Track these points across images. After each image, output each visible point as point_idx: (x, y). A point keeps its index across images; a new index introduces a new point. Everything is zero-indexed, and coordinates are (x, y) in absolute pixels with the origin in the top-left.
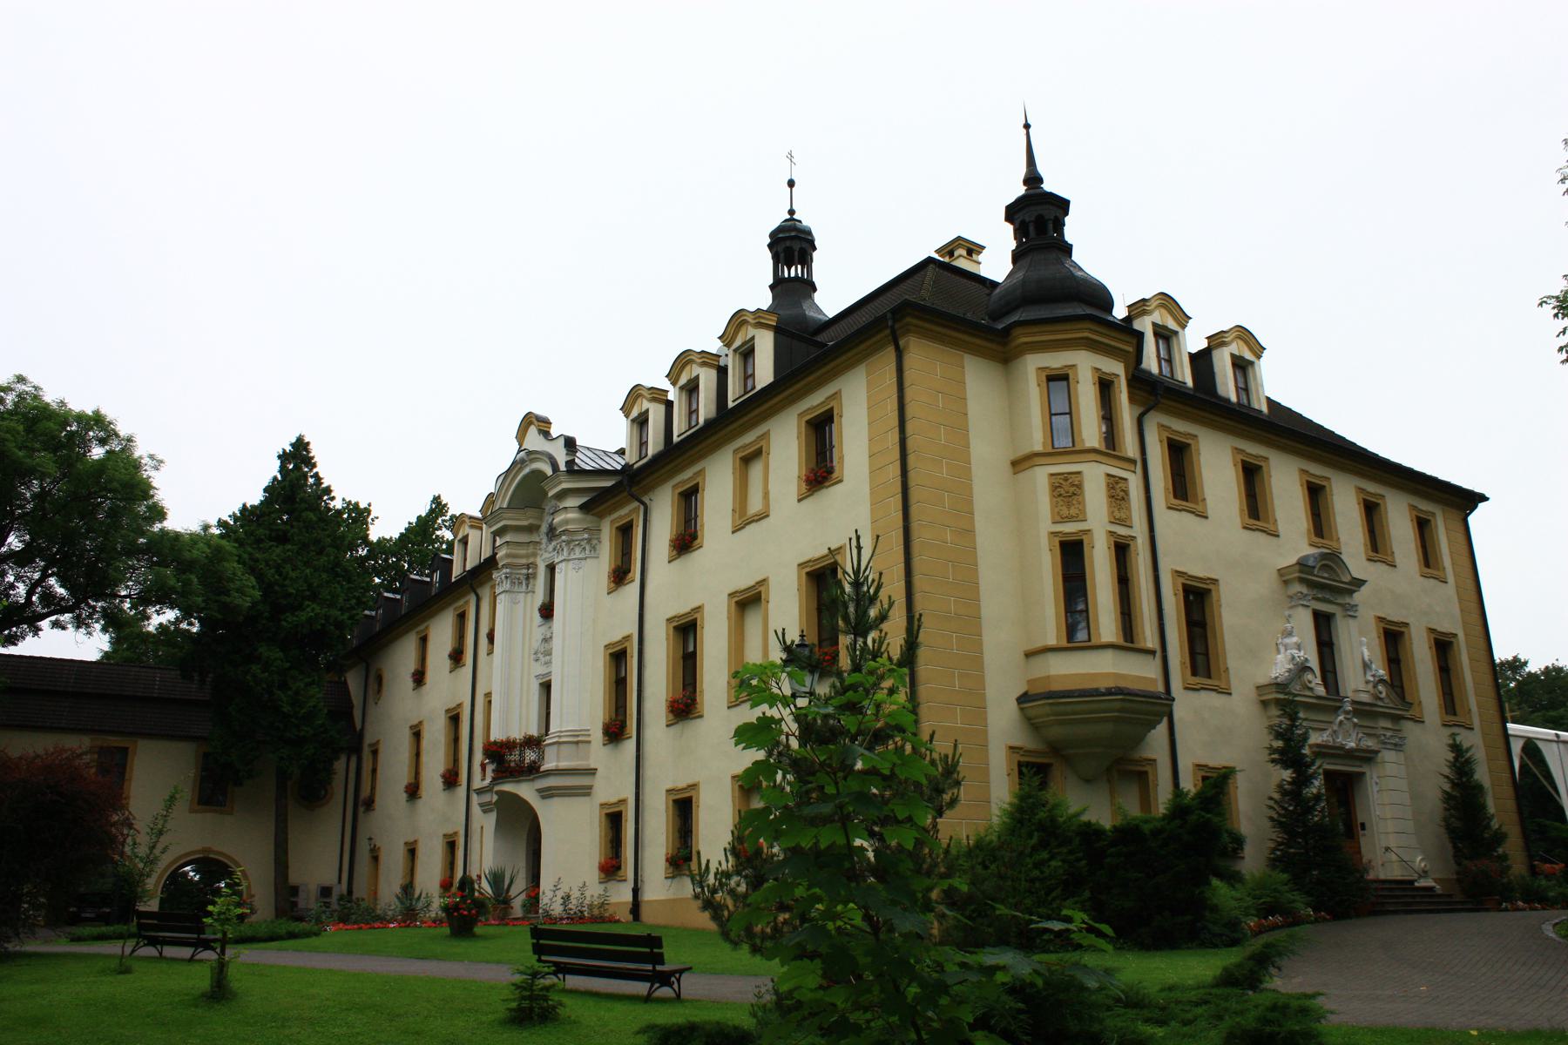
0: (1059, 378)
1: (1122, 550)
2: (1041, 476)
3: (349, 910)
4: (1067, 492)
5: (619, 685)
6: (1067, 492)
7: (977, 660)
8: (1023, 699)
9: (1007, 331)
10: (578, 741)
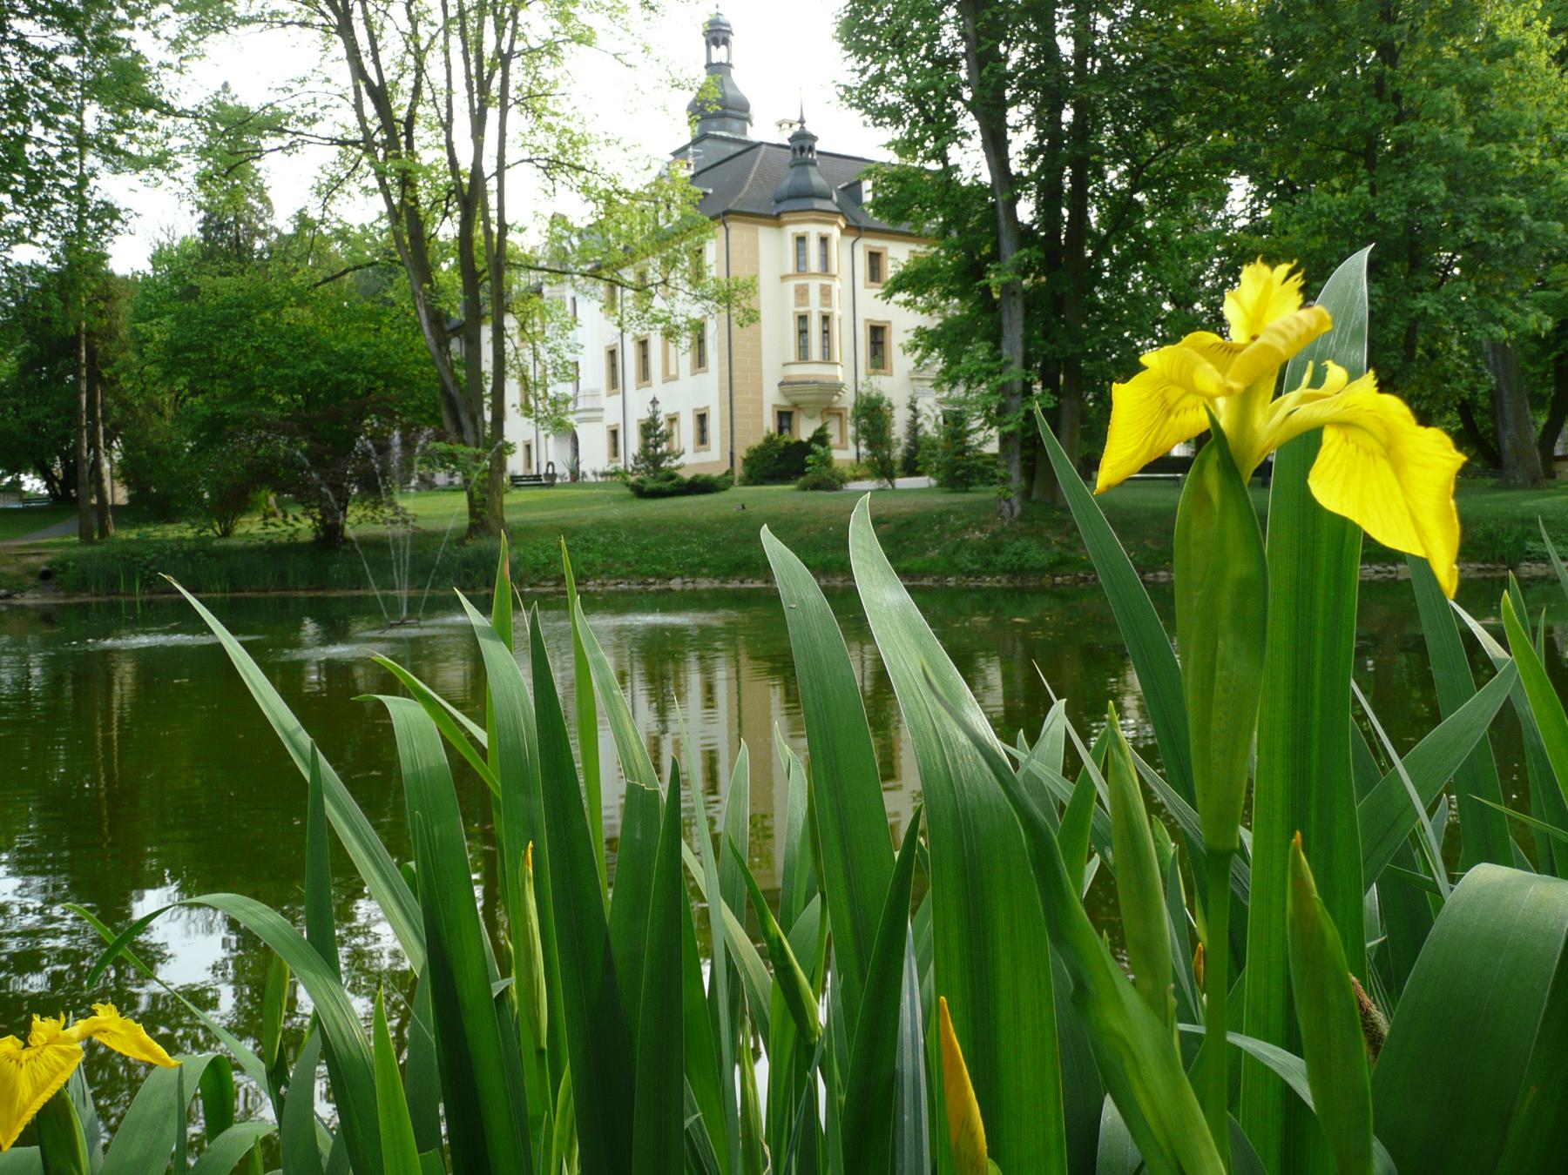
0: (801, 239)
1: (826, 319)
2: (791, 285)
3: (462, 566)
4: (802, 293)
5: (613, 365)
6: (802, 293)
7: (759, 369)
8: (781, 384)
9: (778, 215)
10: (594, 394)
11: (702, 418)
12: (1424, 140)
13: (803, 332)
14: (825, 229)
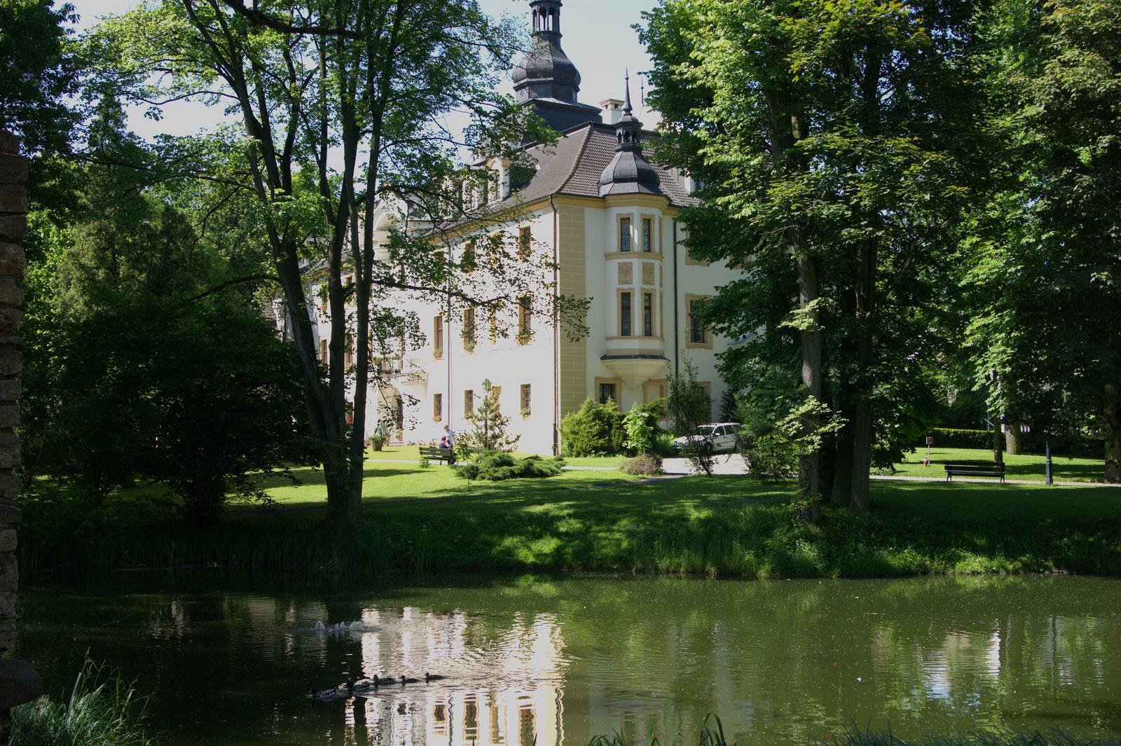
0: (625, 222)
1: (648, 297)
2: (614, 264)
4: (625, 271)
6: (625, 271)
11: (526, 389)
12: (870, 23)
13: (626, 308)
14: (649, 211)
